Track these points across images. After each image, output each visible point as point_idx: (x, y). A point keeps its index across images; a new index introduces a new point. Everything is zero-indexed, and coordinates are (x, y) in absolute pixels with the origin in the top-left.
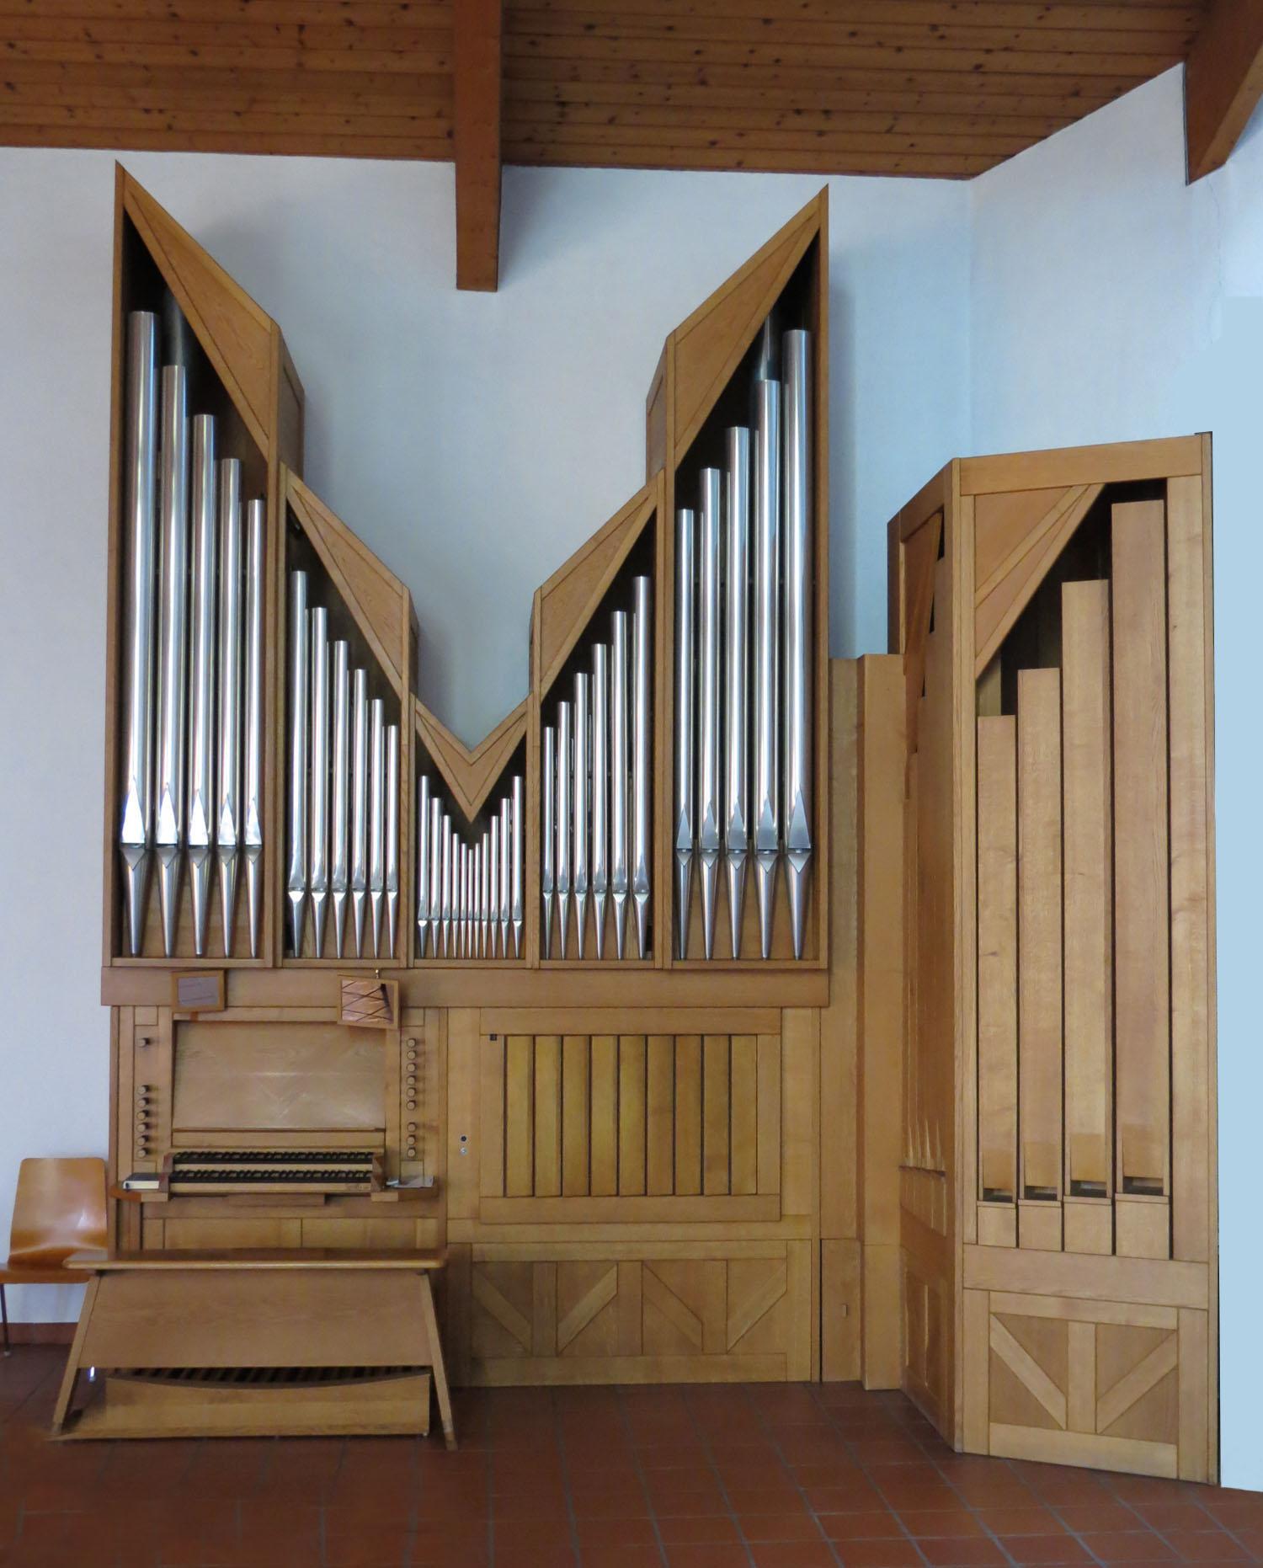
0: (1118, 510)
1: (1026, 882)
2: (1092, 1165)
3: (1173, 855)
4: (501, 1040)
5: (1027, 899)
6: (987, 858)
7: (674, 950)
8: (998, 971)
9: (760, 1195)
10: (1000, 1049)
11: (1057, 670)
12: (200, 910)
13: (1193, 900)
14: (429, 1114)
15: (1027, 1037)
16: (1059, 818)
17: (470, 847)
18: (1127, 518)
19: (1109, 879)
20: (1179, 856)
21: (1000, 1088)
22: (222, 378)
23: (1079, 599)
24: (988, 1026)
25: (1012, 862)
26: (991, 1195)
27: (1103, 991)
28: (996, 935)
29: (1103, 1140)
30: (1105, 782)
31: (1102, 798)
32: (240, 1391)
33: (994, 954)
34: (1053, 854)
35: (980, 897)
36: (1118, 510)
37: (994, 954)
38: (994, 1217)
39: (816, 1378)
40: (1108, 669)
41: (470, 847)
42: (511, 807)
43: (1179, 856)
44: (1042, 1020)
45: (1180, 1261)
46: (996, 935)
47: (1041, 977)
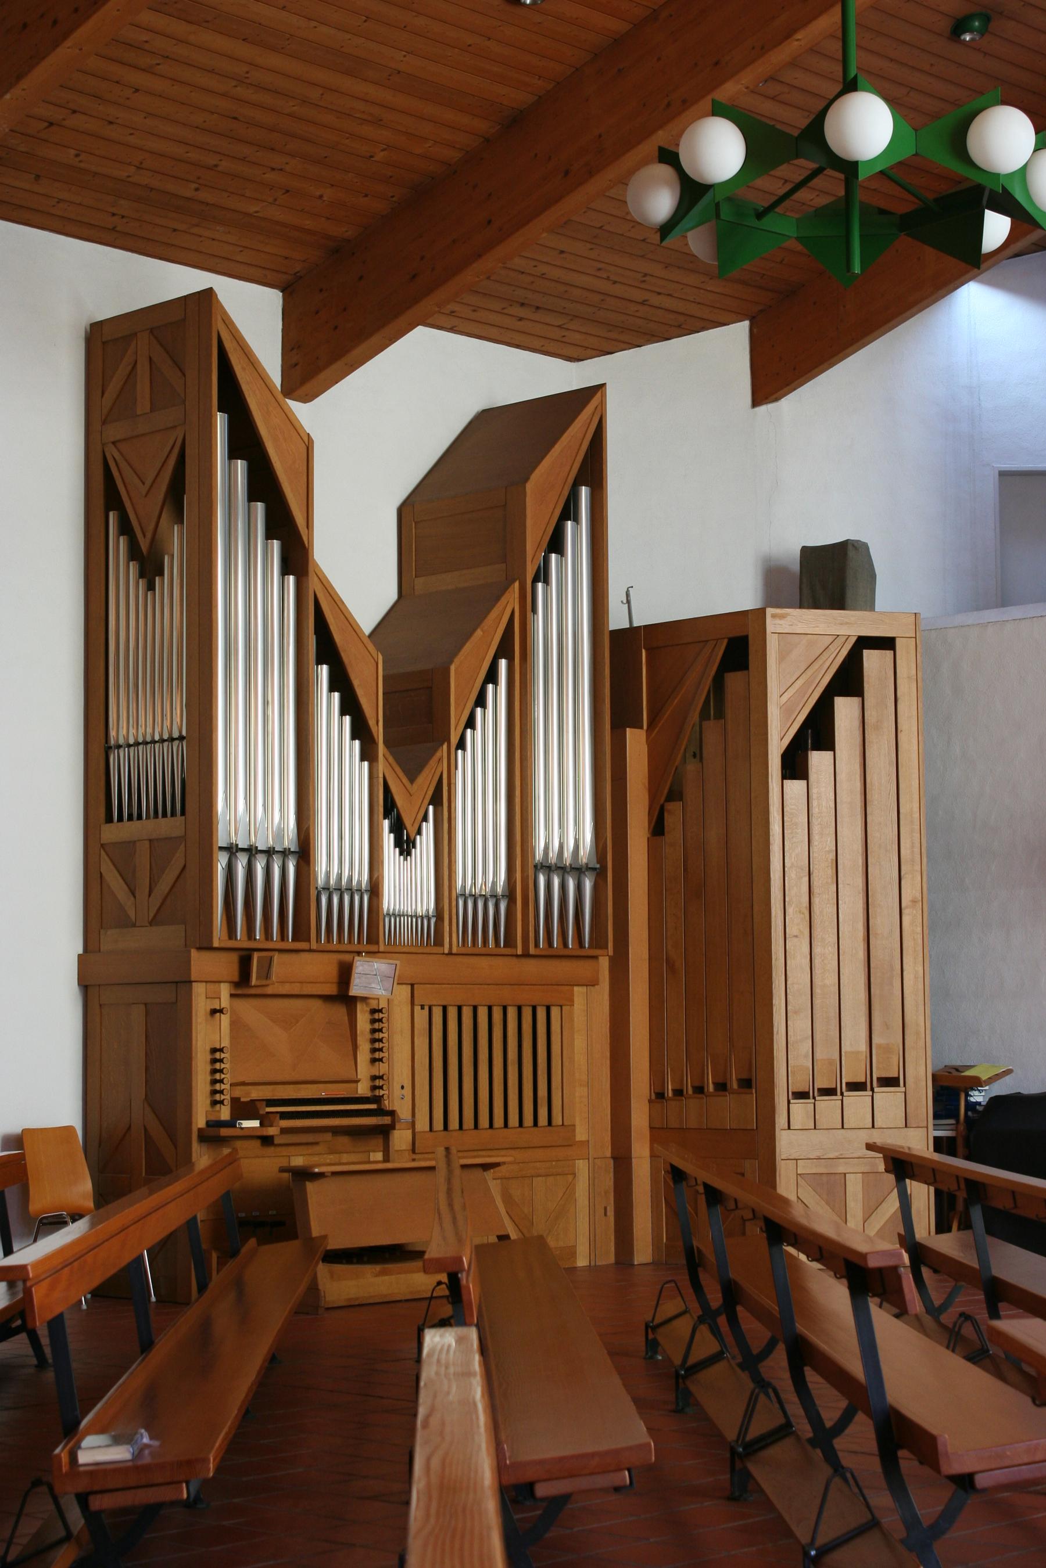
0: (866, 653)
1: (816, 890)
2: (855, 1072)
3: (902, 874)
4: (426, 1008)
5: (816, 900)
6: (791, 874)
7: (384, 943)
8: (799, 949)
9: (566, 1126)
10: (800, 1000)
11: (832, 753)
12: (573, 911)
13: (914, 901)
14: (382, 1068)
15: (817, 991)
16: (834, 848)
17: (405, 859)
18: (871, 659)
19: (865, 888)
20: (906, 874)
21: (800, 1025)
22: (839, 664)
23: (845, 708)
24: (793, 984)
25: (805, 876)
26: (802, 1095)
27: (863, 958)
28: (797, 924)
29: (864, 1057)
30: (861, 827)
31: (860, 836)
32: (386, 1266)
33: (796, 936)
34: (831, 872)
35: (787, 899)
36: (866, 653)
37: (796, 936)
38: (800, 1109)
39: (588, 1264)
40: (862, 754)
41: (405, 859)
42: (427, 827)
43: (906, 874)
44: (826, 979)
45: (911, 1127)
46: (797, 924)
47: (825, 951)
